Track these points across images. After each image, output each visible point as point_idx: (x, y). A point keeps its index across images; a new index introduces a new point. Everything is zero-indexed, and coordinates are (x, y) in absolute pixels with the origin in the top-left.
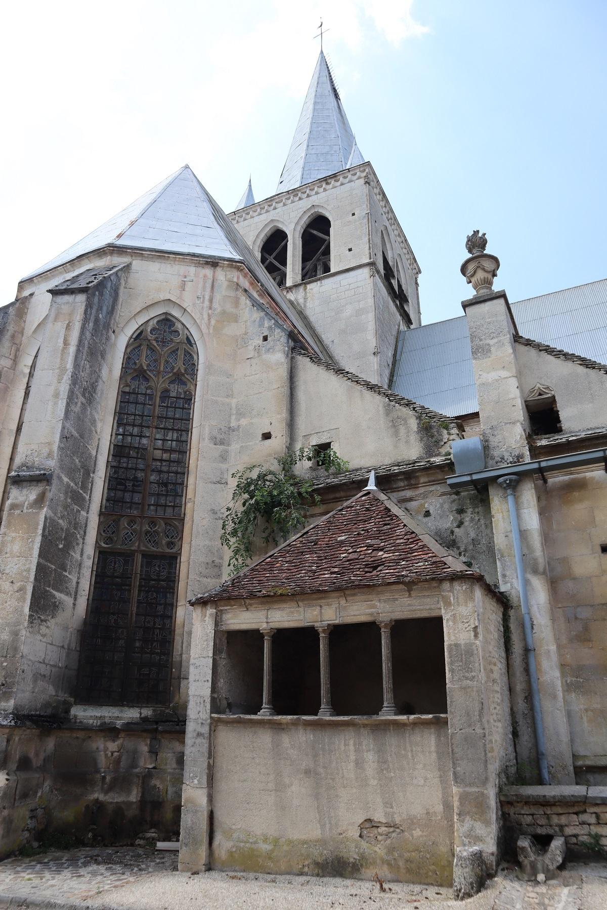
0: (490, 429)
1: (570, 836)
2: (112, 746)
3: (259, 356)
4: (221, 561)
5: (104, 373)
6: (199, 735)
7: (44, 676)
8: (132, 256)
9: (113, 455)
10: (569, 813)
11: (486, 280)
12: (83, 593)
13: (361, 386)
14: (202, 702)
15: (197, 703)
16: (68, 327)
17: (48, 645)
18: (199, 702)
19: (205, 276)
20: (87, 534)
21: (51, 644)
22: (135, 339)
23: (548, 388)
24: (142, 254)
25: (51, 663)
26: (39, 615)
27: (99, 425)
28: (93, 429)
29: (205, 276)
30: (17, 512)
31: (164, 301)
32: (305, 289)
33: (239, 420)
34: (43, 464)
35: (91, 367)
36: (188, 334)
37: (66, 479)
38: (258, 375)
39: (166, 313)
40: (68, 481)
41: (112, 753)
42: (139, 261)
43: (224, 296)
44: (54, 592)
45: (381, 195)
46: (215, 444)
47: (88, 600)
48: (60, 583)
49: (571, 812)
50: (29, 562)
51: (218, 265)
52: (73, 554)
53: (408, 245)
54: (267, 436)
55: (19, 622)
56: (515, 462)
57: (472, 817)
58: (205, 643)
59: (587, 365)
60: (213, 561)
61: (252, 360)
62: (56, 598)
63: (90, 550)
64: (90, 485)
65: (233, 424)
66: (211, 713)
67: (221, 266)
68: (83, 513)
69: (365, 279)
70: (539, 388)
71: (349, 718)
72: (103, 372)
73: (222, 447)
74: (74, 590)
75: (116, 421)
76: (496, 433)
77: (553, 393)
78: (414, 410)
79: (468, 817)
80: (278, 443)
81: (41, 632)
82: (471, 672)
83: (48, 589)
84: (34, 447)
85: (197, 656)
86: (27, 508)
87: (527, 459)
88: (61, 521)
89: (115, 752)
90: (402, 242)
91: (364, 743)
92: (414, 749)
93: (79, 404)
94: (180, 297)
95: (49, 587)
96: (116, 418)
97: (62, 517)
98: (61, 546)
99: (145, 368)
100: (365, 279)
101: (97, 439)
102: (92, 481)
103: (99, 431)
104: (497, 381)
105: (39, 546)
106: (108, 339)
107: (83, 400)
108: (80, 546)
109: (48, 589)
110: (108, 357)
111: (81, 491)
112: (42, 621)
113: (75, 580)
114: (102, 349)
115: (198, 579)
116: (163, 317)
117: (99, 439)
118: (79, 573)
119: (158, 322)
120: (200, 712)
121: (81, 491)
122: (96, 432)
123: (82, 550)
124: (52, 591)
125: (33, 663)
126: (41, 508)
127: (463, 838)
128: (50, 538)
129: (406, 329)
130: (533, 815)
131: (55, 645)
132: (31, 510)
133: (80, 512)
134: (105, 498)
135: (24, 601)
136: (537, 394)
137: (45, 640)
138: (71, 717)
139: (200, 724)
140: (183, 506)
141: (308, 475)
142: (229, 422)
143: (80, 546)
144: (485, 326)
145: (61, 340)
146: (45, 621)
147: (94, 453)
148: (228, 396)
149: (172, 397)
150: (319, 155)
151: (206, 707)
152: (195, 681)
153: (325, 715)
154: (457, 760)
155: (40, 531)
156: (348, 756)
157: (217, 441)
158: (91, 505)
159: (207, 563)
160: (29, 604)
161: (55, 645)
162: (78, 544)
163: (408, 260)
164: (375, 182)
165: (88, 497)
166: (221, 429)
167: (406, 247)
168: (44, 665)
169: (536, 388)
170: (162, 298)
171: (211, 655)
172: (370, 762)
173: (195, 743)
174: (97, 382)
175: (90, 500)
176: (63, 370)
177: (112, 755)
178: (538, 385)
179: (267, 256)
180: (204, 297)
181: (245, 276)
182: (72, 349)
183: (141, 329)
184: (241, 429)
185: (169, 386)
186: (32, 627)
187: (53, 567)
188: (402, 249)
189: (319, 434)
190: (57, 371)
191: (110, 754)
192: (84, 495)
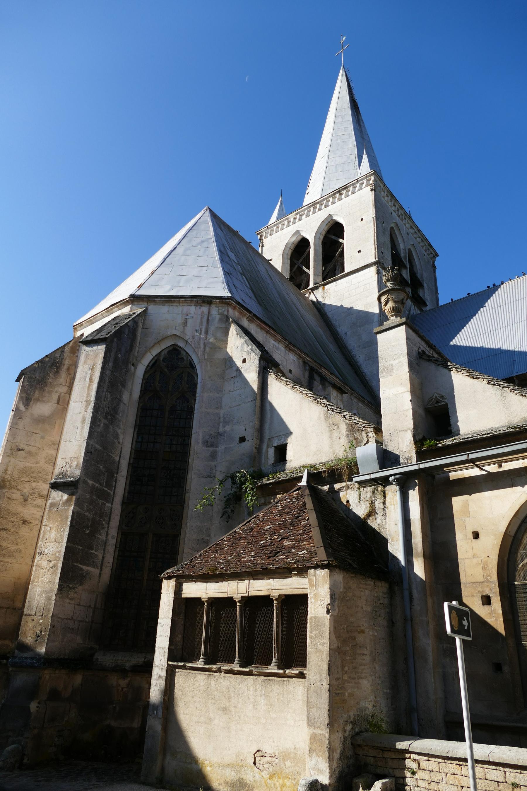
0: (389, 435)
1: (400, 777)
2: (123, 683)
3: (240, 375)
4: (208, 538)
5: (125, 397)
6: (160, 677)
7: (73, 629)
8: (147, 303)
9: (134, 458)
10: (399, 759)
11: (398, 309)
12: (108, 565)
13: (309, 398)
14: (163, 652)
15: (160, 653)
16: (93, 369)
17: (76, 606)
18: (161, 652)
19: (203, 312)
20: (112, 520)
21: (79, 605)
22: (151, 367)
23: (442, 397)
24: (155, 300)
25: (79, 619)
26: (68, 584)
27: (121, 437)
28: (116, 441)
29: (203, 312)
30: (55, 509)
31: (171, 336)
32: (324, 289)
33: (225, 427)
34: (73, 473)
35: (111, 395)
36: (191, 360)
37: (91, 482)
38: (238, 391)
39: (174, 345)
40: (93, 483)
41: (122, 689)
42: (153, 306)
43: (217, 328)
44: (82, 566)
45: (390, 197)
46: (207, 447)
47: (112, 569)
48: (88, 559)
49: (400, 757)
50: (60, 545)
51: (212, 303)
52: (99, 536)
53: (422, 234)
54: (242, 440)
55: (52, 590)
56: (405, 464)
57: (317, 754)
58: (168, 607)
59: (473, 376)
60: (203, 539)
61: (235, 378)
62: (83, 570)
63: (113, 532)
64: (114, 483)
65: (221, 430)
66: (168, 660)
67: (214, 304)
68: (109, 505)
69: (372, 277)
70: (436, 397)
71: (249, 670)
72: (124, 397)
73: (211, 449)
74: (100, 563)
75: (136, 432)
76: (392, 439)
77: (446, 401)
78: (344, 417)
79: (315, 753)
80: (248, 446)
81: (69, 596)
82: (323, 639)
83: (75, 564)
84: (68, 460)
85: (162, 617)
86: (61, 506)
87: (414, 461)
88: (87, 514)
89: (125, 688)
90: (415, 232)
91: (260, 689)
92: (289, 697)
93: (102, 425)
94: (183, 332)
95: (77, 563)
96: (137, 430)
97: (88, 511)
98: (87, 532)
99: (158, 389)
100: (372, 277)
101: (120, 448)
102: (116, 480)
103: (121, 441)
104: (396, 395)
105: (68, 534)
106: (127, 371)
107: (106, 421)
108: (106, 529)
109: (75, 564)
110: (129, 384)
111: (106, 489)
112: (70, 588)
113: (101, 556)
114: (122, 379)
115: (191, 553)
116: (172, 348)
117: (122, 448)
118: (104, 550)
119: (169, 352)
120: (161, 659)
121: (106, 489)
122: (119, 443)
123: (107, 532)
124: (79, 565)
125: (63, 619)
126: (70, 506)
127: (311, 770)
128: (77, 527)
129: (419, 312)
130: (375, 757)
131: (82, 606)
132: (63, 507)
133: (105, 504)
134: (127, 491)
135: (56, 575)
136: (435, 402)
137: (73, 602)
138: (94, 660)
139: (161, 669)
140: (184, 495)
141: (270, 470)
142: (218, 428)
143: (106, 529)
144: (390, 349)
145: (88, 379)
146: (74, 588)
147: (117, 459)
148: (217, 408)
149: (178, 411)
150: (338, 166)
151: (165, 656)
152: (160, 636)
153: (236, 667)
154: (310, 708)
155: (69, 523)
156: (249, 699)
157: (208, 444)
158: (115, 498)
159: (198, 540)
160: (59, 577)
161: (82, 606)
162: (103, 528)
163: (423, 247)
164: (382, 186)
165: (112, 493)
166: (211, 435)
167: (420, 236)
168: (73, 622)
169: (434, 397)
170: (170, 334)
171: (171, 617)
172: (262, 704)
173: (157, 683)
174: (118, 405)
175: (114, 494)
176: (88, 402)
177: (122, 690)
178: (436, 395)
179: (296, 261)
180: (201, 330)
181: (234, 308)
182: (95, 386)
183: (156, 358)
184: (225, 434)
185: (176, 402)
186: (61, 593)
187: (81, 548)
188: (416, 238)
189: (279, 437)
190: (85, 402)
191: (120, 689)
192: (109, 491)
